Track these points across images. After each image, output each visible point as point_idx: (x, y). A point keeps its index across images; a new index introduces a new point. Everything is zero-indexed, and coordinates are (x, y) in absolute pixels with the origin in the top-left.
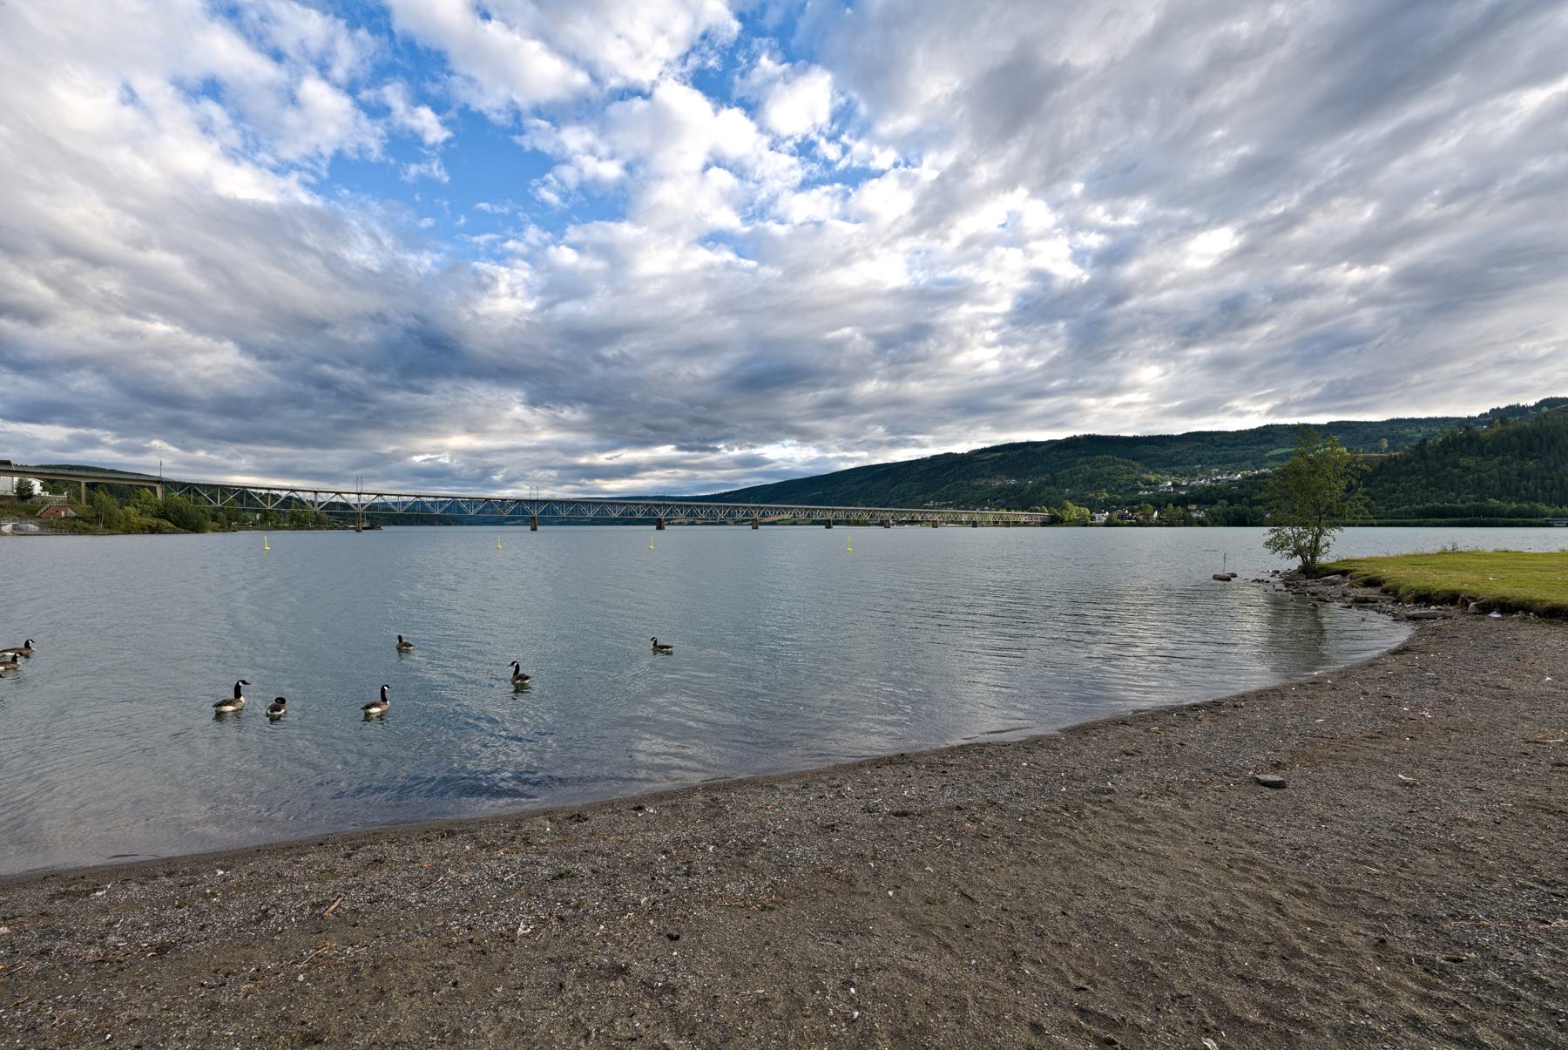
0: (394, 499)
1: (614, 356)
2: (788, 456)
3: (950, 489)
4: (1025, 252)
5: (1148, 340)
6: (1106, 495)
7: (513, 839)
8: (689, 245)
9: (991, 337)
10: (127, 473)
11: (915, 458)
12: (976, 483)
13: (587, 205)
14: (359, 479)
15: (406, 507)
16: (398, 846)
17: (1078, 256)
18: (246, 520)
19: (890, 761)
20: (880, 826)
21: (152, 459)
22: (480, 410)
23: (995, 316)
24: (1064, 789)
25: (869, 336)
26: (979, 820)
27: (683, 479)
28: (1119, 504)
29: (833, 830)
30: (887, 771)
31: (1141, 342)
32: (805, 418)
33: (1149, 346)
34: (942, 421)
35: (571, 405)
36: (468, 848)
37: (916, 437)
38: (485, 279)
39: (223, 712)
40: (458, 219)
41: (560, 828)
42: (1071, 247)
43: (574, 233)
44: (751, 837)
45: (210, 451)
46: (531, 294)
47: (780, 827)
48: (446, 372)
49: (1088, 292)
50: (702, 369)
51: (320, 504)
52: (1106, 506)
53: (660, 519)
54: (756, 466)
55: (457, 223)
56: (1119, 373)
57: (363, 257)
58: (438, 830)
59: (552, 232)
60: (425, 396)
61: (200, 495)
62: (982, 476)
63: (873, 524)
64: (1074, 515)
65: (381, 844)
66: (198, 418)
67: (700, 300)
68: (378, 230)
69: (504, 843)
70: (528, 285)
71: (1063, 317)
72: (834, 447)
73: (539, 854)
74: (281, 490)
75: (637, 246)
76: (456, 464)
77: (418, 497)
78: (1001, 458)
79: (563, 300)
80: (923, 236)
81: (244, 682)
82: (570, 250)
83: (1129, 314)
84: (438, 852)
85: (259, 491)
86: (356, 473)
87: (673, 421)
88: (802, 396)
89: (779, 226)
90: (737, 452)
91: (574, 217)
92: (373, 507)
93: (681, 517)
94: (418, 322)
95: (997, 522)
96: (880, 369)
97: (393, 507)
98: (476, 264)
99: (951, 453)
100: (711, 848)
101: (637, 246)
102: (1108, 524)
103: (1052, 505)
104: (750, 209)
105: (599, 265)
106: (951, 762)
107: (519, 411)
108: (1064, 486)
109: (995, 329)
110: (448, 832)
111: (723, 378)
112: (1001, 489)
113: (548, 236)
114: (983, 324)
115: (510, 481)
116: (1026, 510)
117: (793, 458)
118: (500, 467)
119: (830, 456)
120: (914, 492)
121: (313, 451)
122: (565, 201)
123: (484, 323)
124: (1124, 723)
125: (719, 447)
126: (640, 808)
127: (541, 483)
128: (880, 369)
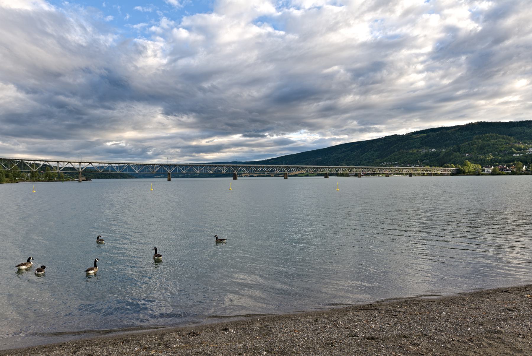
0: (98, 165)
1: (209, 87)
2: (303, 139)
5: (520, 64)
6: (492, 157)
7: (159, 344)
8: (247, 24)
9: (420, 67)
11: (375, 138)
12: (411, 151)
13: (193, 5)
14: (80, 155)
15: (104, 169)
17: (475, 16)
18: (23, 177)
19: (364, 308)
20: (359, 345)
22: (140, 118)
23: (422, 55)
24: (469, 329)
25: (348, 70)
26: (417, 345)
27: (246, 152)
28: (500, 162)
29: (332, 346)
30: (362, 313)
31: (515, 65)
32: (312, 117)
33: (520, 67)
34: (391, 117)
35: (187, 114)
36: (136, 349)
37: (376, 126)
38: (140, 48)
40: (126, 16)
41: (184, 339)
42: (470, 11)
43: (186, 21)
44: (286, 347)
46: (165, 56)
47: (302, 343)
49: (480, 37)
50: (256, 92)
51: (60, 168)
52: (492, 163)
53: (235, 174)
55: (125, 18)
56: (500, 84)
57: (77, 38)
58: (121, 339)
59: (175, 21)
60: (112, 111)
62: (415, 147)
63: (351, 176)
64: (472, 169)
67: (253, 56)
68: (84, 24)
70: (163, 50)
71: (464, 53)
72: (329, 133)
73: (173, 353)
74: (40, 161)
76: (129, 146)
77: (110, 164)
79: (181, 58)
80: (379, 11)
81: (100, 236)
82: (185, 30)
83: (507, 48)
84: (121, 351)
85: (29, 162)
86: (78, 151)
87: (240, 121)
90: (275, 137)
92: (87, 169)
93: (246, 172)
94: (107, 72)
95: (424, 174)
96: (354, 88)
97: (97, 169)
98: (135, 40)
100: (264, 353)
102: (493, 173)
103: (457, 163)
105: (200, 38)
106: (399, 310)
107: (160, 117)
108: (465, 152)
109: (422, 62)
110: (126, 340)
111: (267, 96)
112: (426, 155)
113: (172, 23)
114: (415, 60)
115: (156, 155)
116: (441, 166)
117: (306, 140)
119: (327, 138)
120: (375, 157)
121: (55, 140)
123: (141, 71)
124: (507, 291)
125: (265, 134)
126: (226, 330)
127: (173, 156)
128: (354, 88)
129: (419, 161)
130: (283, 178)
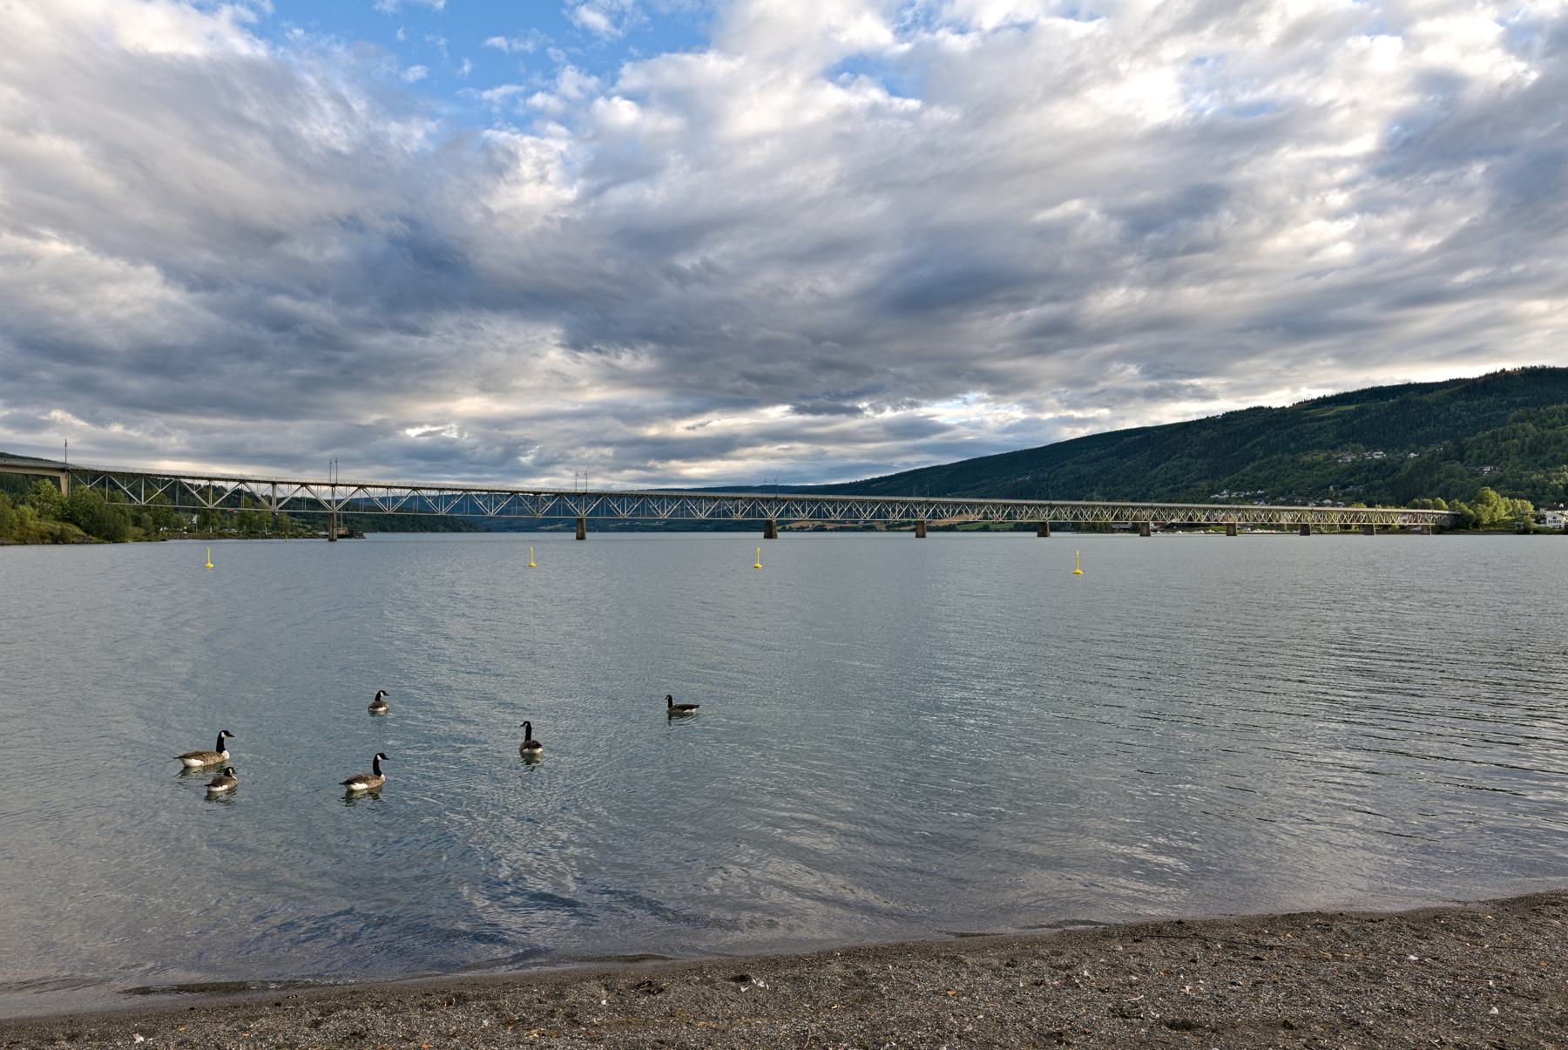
0: (381, 492)
1: (694, 267)
2: (974, 419)
3: (1259, 469)
4: (1407, 39)
7: (552, 1013)
8: (810, 81)
10: (22, 458)
11: (1194, 418)
12: (1307, 458)
14: (334, 464)
15: (399, 505)
16: (384, 1013)
21: (51, 438)
22: (500, 358)
23: (1346, 161)
24: (1495, 1011)
25: (1111, 213)
27: (803, 458)
29: (1060, 1042)
30: (1153, 947)
32: (1001, 355)
34: (1245, 352)
35: (632, 348)
37: (1198, 382)
38: (500, 157)
39: (213, 792)
40: (461, 65)
41: (622, 1002)
42: (1501, 22)
43: (632, 76)
45: (128, 424)
47: (970, 1028)
48: (447, 301)
50: (831, 282)
51: (279, 500)
53: (770, 523)
54: (921, 435)
55: (459, 72)
57: (326, 132)
58: (443, 992)
61: (117, 488)
62: (1321, 446)
65: (362, 1010)
66: (109, 377)
68: (345, 91)
69: (540, 1020)
71: (1479, 155)
72: (1053, 401)
74: (226, 480)
75: (728, 89)
76: (468, 439)
77: (415, 489)
78: (1355, 414)
79: (616, 183)
80: (1208, 32)
82: (627, 103)
85: (197, 482)
86: (328, 454)
88: (997, 318)
89: (957, 37)
90: (889, 414)
91: (631, 49)
92: (352, 505)
93: (803, 518)
94: (406, 227)
95: (1349, 527)
96: (1130, 267)
97: (381, 505)
98: (488, 133)
99: (1261, 408)
101: (728, 89)
103: (1456, 496)
104: (909, 13)
105: (671, 123)
106: (1270, 942)
107: (555, 356)
108: (1482, 461)
109: (1344, 186)
110: (458, 996)
112: (1355, 469)
113: (592, 82)
114: (1323, 178)
115: (545, 465)
117: (982, 422)
118: (529, 443)
119: (1047, 416)
121: (266, 423)
122: (617, 23)
123: (500, 224)
125: (860, 406)
126: (743, 979)
127: (591, 468)
128: (1130, 267)
129: (1331, 488)
130: (914, 534)
